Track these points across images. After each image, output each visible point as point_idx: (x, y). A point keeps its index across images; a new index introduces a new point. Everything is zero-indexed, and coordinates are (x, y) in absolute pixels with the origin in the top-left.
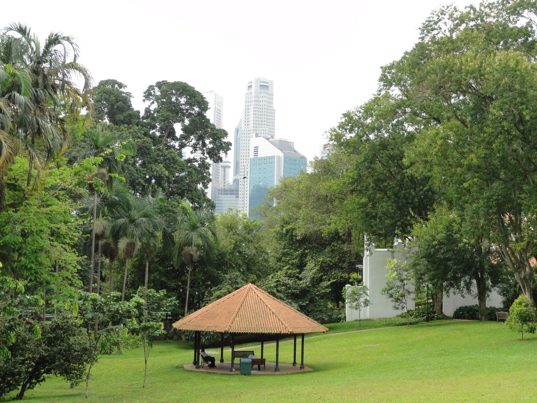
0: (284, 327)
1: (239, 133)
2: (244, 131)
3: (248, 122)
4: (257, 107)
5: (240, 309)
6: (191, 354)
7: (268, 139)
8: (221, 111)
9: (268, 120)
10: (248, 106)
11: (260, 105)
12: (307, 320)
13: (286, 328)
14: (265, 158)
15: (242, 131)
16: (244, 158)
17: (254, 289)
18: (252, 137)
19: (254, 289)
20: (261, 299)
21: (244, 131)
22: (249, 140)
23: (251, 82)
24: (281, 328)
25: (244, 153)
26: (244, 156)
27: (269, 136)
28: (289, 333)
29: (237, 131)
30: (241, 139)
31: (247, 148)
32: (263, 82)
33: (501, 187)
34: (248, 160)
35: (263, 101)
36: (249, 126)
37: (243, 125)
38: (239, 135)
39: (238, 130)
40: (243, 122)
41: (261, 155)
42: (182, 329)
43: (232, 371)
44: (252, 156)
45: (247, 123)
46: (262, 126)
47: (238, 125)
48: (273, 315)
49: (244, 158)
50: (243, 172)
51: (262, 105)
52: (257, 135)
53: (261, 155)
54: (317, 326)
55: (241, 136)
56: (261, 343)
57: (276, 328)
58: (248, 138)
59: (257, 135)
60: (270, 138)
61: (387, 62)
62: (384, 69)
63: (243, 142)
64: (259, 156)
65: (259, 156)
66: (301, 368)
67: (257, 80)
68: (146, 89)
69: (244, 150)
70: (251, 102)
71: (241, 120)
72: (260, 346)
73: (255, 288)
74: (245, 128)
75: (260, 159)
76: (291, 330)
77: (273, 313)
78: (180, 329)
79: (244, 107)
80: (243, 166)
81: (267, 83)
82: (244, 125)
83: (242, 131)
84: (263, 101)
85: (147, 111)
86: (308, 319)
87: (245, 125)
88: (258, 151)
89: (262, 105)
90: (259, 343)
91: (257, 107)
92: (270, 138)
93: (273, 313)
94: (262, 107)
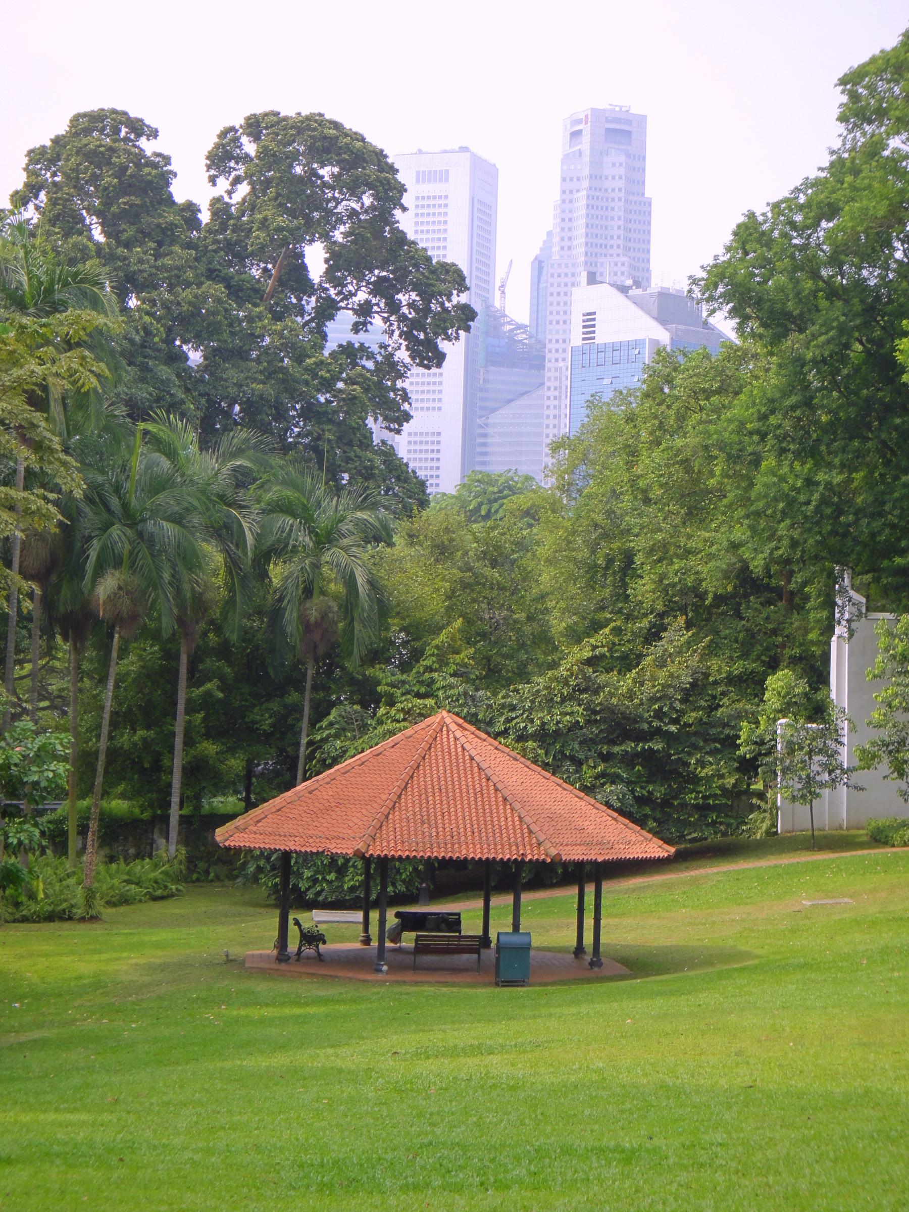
0: (534, 840)
1: (545, 271)
2: (559, 265)
3: (570, 239)
4: (598, 194)
5: (406, 787)
6: (273, 921)
7: (624, 290)
8: (490, 207)
9: (630, 235)
10: (571, 192)
11: (606, 190)
12: (611, 822)
13: (539, 844)
14: (616, 348)
15: (552, 265)
16: (557, 346)
17: (453, 727)
18: (579, 284)
19: (453, 727)
20: (472, 759)
21: (559, 265)
22: (566, 294)
23: (579, 122)
24: (524, 845)
25: (558, 331)
26: (557, 341)
27: (629, 282)
28: (549, 860)
29: (539, 266)
30: (551, 290)
31: (561, 318)
32: (617, 120)
33: (788, 402)
34: (564, 351)
35: (614, 178)
36: (574, 252)
37: (556, 249)
38: (543, 278)
39: (540, 262)
40: (556, 239)
41: (603, 337)
42: (232, 844)
43: (381, 971)
44: (576, 339)
45: (566, 244)
46: (611, 251)
47: (541, 249)
48: (505, 805)
49: (557, 346)
50: (556, 389)
51: (613, 190)
52: (592, 279)
53: (603, 337)
54: (641, 838)
55: (551, 280)
56: (483, 893)
57: (510, 844)
58: (562, 289)
59: (592, 279)
60: (630, 287)
61: (859, 57)
62: (850, 80)
63: (555, 299)
64: (597, 341)
65: (597, 341)
66: (592, 964)
67: (596, 113)
68: (210, 141)
69: (558, 322)
70: (578, 179)
71: (550, 234)
72: (480, 903)
73: (459, 725)
74: (562, 256)
75: (602, 349)
76: (553, 852)
77: (505, 799)
78: (227, 844)
79: (557, 196)
80: (556, 369)
81: (629, 122)
82: (558, 248)
83: (552, 265)
84: (614, 178)
85: (219, 208)
86: (614, 819)
87: (562, 248)
88: (594, 326)
89: (613, 190)
90: (478, 893)
91: (598, 194)
92: (630, 287)
93: (505, 799)
94: (613, 195)
